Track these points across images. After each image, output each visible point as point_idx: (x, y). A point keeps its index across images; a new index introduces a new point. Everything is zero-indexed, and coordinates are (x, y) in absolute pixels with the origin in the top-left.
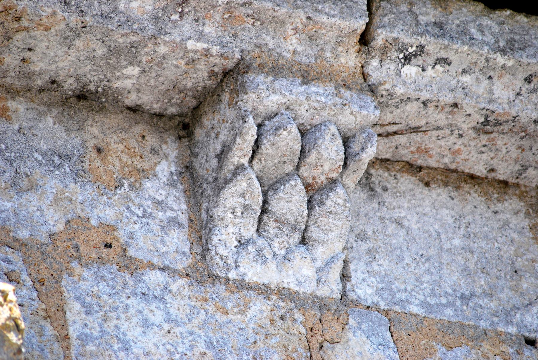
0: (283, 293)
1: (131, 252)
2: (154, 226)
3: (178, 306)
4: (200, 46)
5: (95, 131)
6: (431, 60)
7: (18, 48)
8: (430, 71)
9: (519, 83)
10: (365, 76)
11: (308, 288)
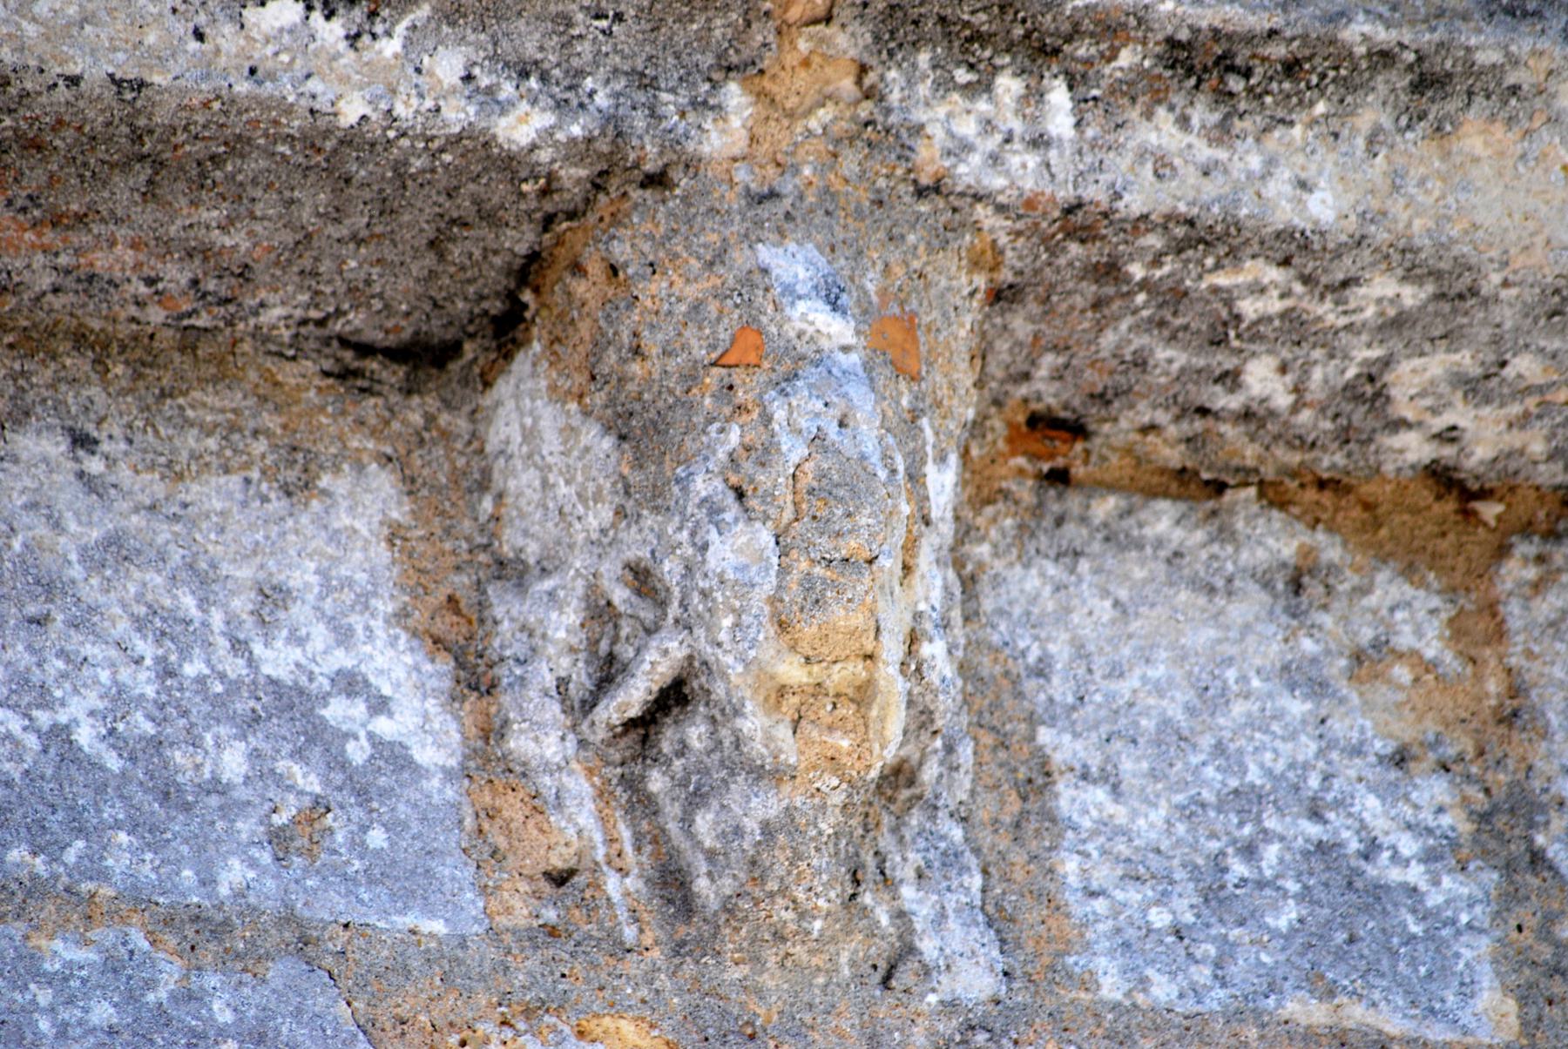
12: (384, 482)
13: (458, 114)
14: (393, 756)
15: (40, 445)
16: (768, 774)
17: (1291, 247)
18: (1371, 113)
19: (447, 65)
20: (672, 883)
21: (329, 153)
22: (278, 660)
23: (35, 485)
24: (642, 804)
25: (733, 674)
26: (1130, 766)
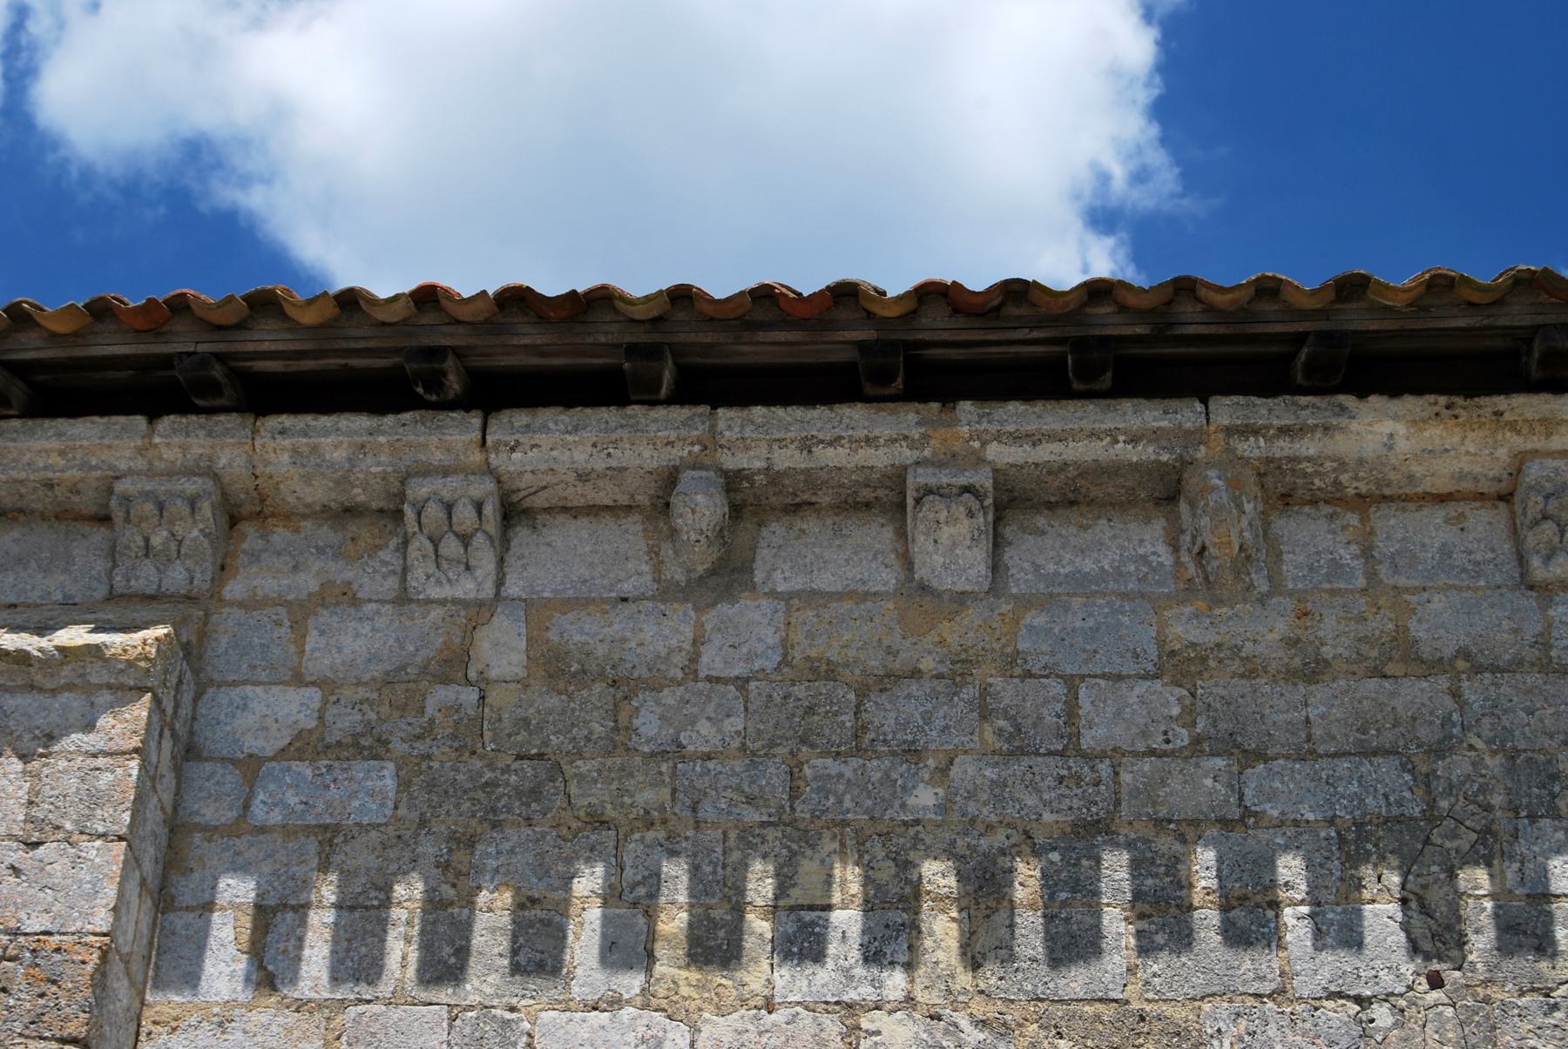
0: (456, 601)
1: (359, 595)
2: (378, 577)
3: (381, 622)
4: (380, 469)
5: (354, 528)
6: (527, 447)
7: (662, 506)
8: (530, 454)
9: (589, 449)
10: (488, 464)
11: (472, 596)
12: (1163, 520)
13: (1153, 457)
14: (1161, 564)
15: (1103, 522)
16: (1216, 558)
17: (1309, 459)
18: (1318, 435)
19: (1150, 449)
20: (1207, 578)
21: (1135, 467)
22: (1141, 551)
23: (4, 424)
24: (1202, 566)
25: (1208, 544)
26: (1297, 550)
